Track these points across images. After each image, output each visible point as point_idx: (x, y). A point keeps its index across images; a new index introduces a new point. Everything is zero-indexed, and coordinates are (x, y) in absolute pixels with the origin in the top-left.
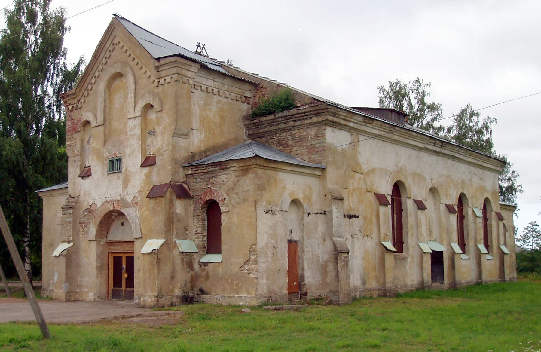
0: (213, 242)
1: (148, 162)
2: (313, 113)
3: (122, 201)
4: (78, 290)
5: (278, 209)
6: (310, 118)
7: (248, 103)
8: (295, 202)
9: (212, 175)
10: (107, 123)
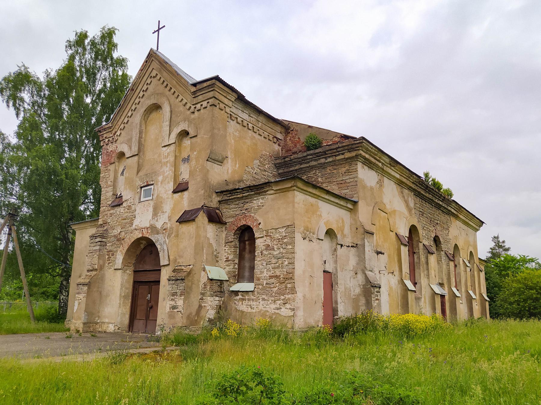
0: (244, 268)
1: (181, 188)
2: (346, 148)
3: (153, 228)
4: (99, 321)
5: (315, 236)
6: (343, 154)
7: (279, 145)
8: (330, 233)
9: (247, 200)
10: (141, 154)
